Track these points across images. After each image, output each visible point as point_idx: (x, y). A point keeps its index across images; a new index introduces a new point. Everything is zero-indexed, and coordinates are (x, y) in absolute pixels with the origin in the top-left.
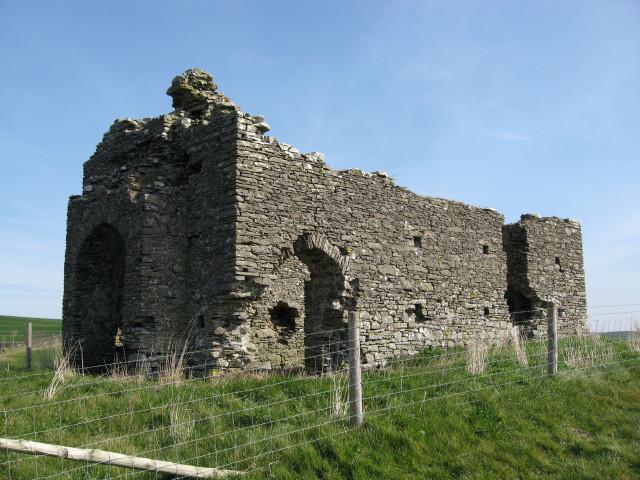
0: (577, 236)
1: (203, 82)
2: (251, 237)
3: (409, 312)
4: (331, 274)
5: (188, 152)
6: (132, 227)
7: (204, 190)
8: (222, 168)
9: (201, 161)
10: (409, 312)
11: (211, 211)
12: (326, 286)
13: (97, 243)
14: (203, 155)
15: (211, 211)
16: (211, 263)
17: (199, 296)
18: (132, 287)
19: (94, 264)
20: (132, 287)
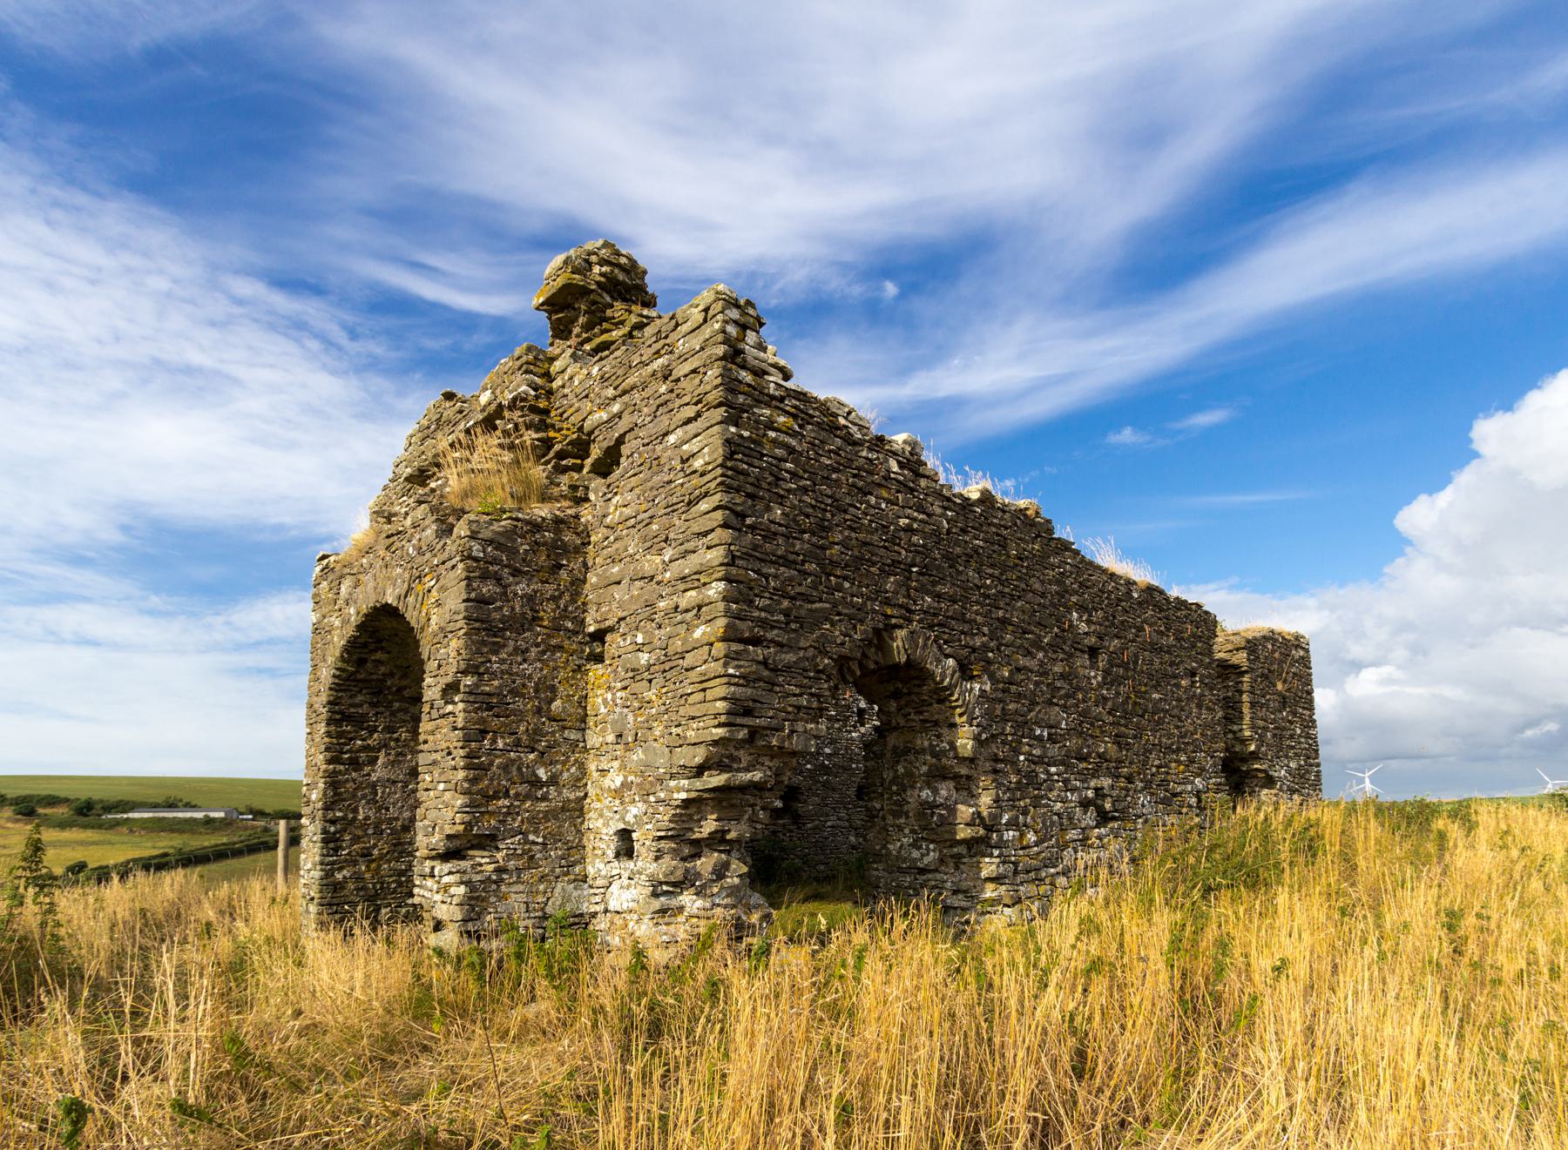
0: (1305, 662)
1: (556, 594)
2: (764, 623)
3: (1085, 804)
4: (936, 723)
5: (588, 425)
6: (438, 604)
7: (628, 511)
8: (677, 446)
9: (620, 441)
10: (1085, 804)
11: (650, 564)
12: (923, 751)
13: (379, 655)
14: (622, 426)
15: (650, 564)
16: (650, 695)
17: (619, 781)
18: (438, 756)
19: (372, 705)
20: (438, 756)
